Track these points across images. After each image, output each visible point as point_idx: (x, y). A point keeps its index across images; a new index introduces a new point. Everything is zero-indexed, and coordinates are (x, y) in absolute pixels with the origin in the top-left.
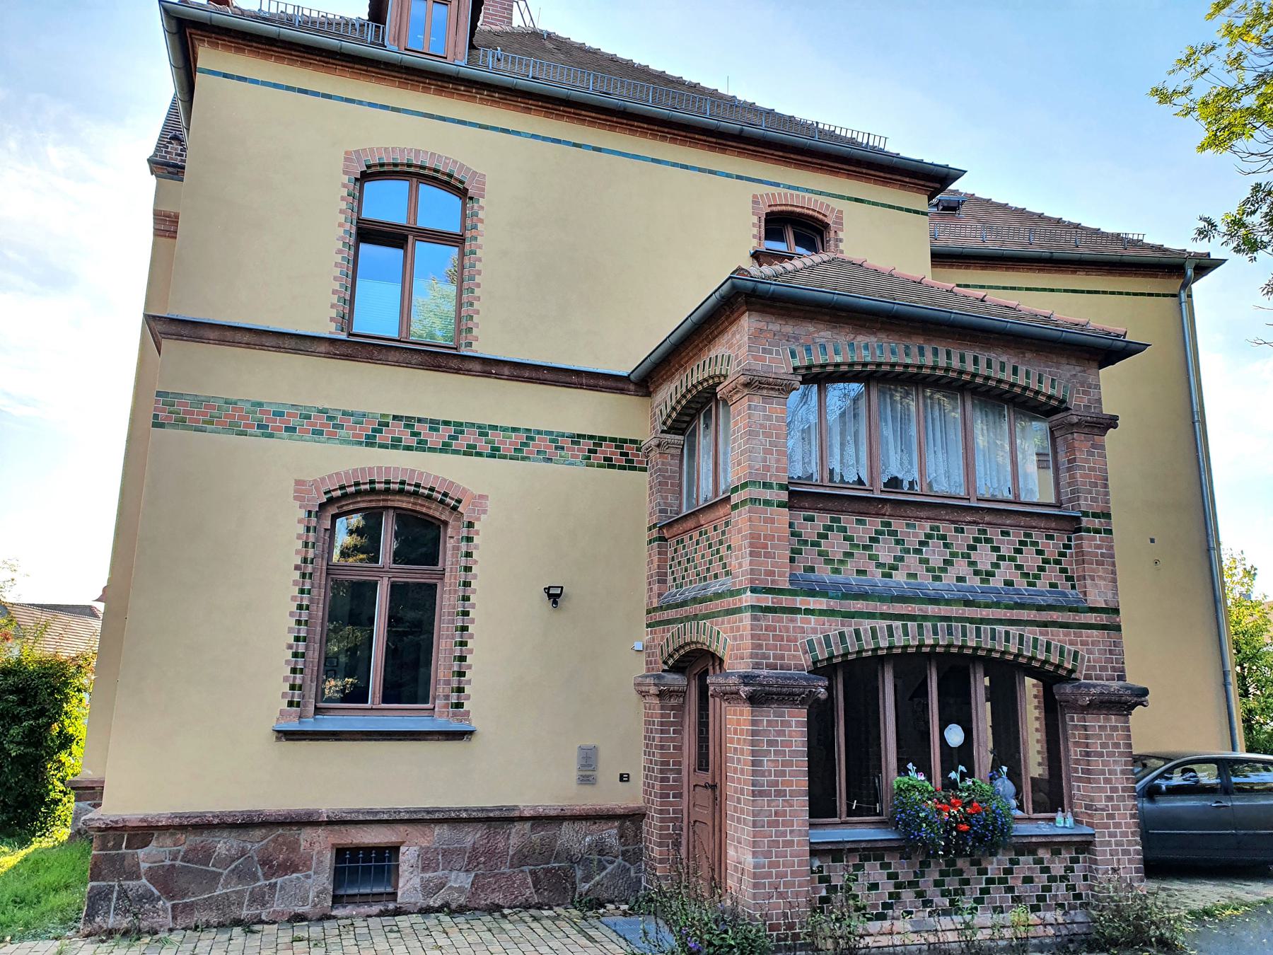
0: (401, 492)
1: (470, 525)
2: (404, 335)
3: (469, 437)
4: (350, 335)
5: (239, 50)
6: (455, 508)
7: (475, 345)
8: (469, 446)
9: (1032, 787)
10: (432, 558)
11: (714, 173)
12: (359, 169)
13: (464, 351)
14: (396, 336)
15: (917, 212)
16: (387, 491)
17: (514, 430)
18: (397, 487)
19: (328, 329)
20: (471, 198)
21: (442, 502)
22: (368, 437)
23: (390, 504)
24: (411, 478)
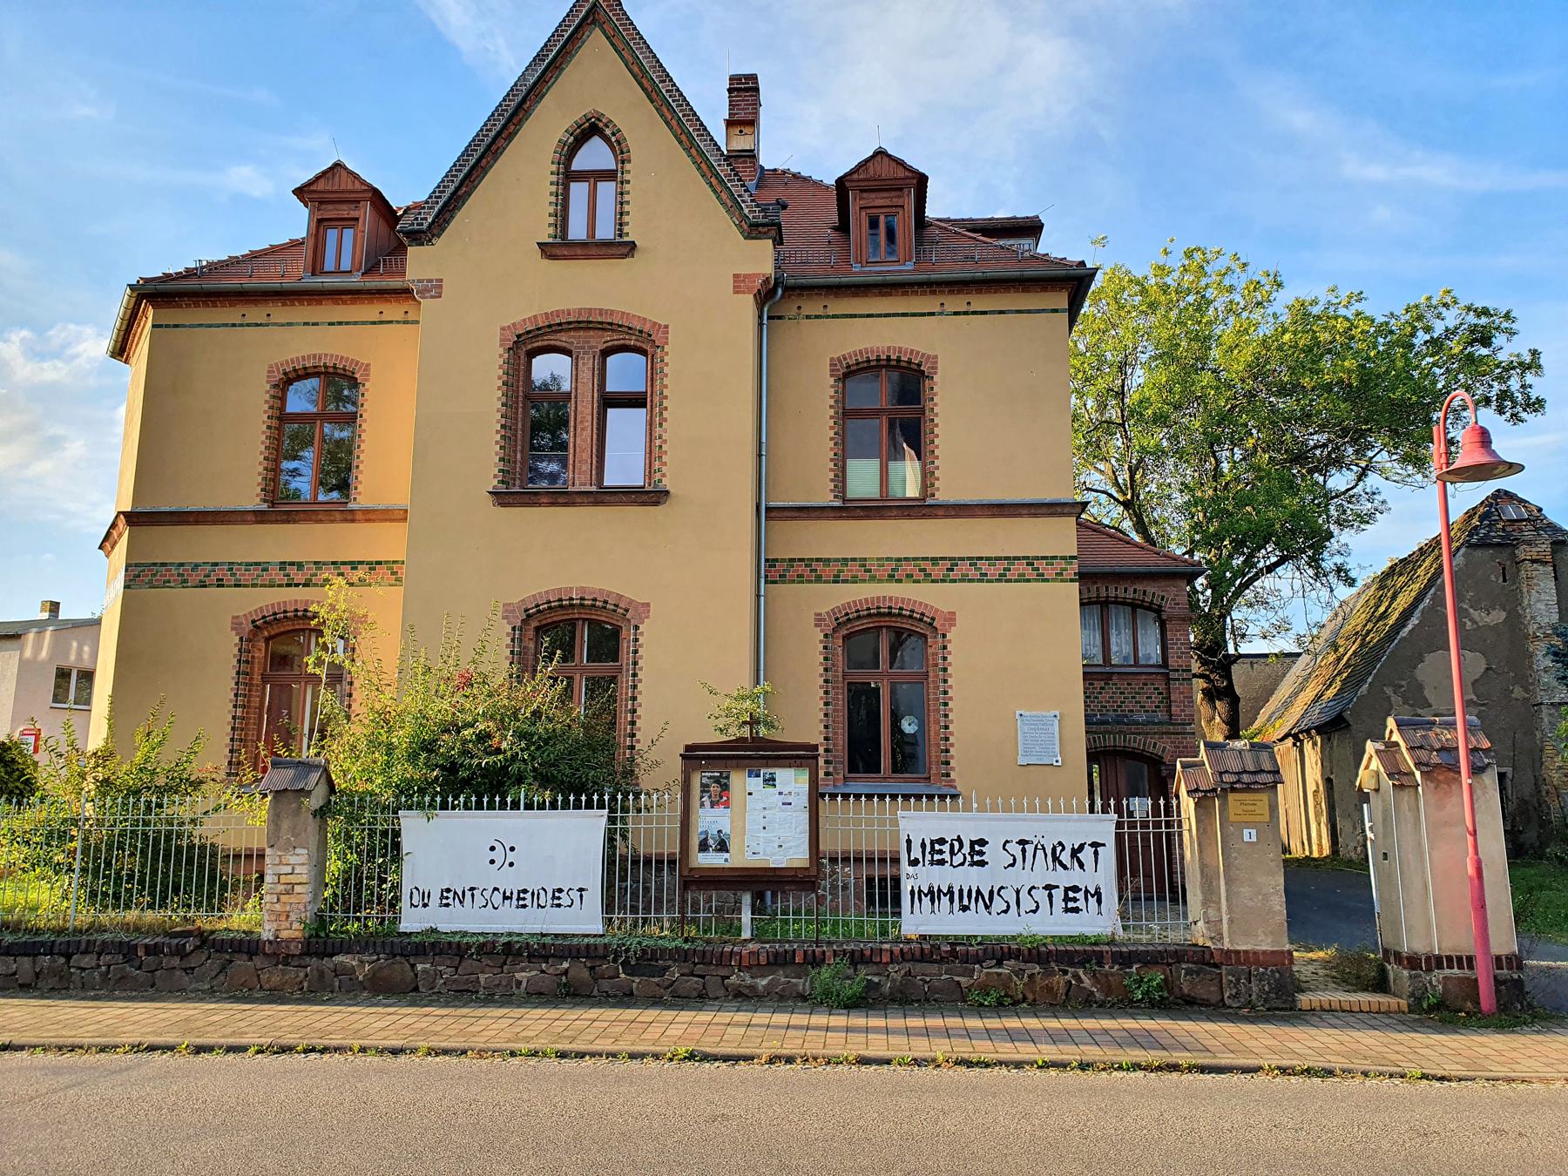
0: (859, 617)
1: (944, 636)
2: (884, 495)
3: (964, 567)
4: (844, 500)
5: (197, 305)
6: (931, 624)
7: (937, 494)
8: (356, 568)
9: (1512, 835)
10: (614, 655)
11: (855, 316)
12: (278, 376)
13: (929, 501)
14: (877, 496)
15: (257, 325)
16: (890, 614)
17: (888, 559)
18: (601, 604)
19: (827, 498)
20: (927, 377)
21: (921, 620)
22: (889, 576)
23: (882, 624)
24: (873, 604)
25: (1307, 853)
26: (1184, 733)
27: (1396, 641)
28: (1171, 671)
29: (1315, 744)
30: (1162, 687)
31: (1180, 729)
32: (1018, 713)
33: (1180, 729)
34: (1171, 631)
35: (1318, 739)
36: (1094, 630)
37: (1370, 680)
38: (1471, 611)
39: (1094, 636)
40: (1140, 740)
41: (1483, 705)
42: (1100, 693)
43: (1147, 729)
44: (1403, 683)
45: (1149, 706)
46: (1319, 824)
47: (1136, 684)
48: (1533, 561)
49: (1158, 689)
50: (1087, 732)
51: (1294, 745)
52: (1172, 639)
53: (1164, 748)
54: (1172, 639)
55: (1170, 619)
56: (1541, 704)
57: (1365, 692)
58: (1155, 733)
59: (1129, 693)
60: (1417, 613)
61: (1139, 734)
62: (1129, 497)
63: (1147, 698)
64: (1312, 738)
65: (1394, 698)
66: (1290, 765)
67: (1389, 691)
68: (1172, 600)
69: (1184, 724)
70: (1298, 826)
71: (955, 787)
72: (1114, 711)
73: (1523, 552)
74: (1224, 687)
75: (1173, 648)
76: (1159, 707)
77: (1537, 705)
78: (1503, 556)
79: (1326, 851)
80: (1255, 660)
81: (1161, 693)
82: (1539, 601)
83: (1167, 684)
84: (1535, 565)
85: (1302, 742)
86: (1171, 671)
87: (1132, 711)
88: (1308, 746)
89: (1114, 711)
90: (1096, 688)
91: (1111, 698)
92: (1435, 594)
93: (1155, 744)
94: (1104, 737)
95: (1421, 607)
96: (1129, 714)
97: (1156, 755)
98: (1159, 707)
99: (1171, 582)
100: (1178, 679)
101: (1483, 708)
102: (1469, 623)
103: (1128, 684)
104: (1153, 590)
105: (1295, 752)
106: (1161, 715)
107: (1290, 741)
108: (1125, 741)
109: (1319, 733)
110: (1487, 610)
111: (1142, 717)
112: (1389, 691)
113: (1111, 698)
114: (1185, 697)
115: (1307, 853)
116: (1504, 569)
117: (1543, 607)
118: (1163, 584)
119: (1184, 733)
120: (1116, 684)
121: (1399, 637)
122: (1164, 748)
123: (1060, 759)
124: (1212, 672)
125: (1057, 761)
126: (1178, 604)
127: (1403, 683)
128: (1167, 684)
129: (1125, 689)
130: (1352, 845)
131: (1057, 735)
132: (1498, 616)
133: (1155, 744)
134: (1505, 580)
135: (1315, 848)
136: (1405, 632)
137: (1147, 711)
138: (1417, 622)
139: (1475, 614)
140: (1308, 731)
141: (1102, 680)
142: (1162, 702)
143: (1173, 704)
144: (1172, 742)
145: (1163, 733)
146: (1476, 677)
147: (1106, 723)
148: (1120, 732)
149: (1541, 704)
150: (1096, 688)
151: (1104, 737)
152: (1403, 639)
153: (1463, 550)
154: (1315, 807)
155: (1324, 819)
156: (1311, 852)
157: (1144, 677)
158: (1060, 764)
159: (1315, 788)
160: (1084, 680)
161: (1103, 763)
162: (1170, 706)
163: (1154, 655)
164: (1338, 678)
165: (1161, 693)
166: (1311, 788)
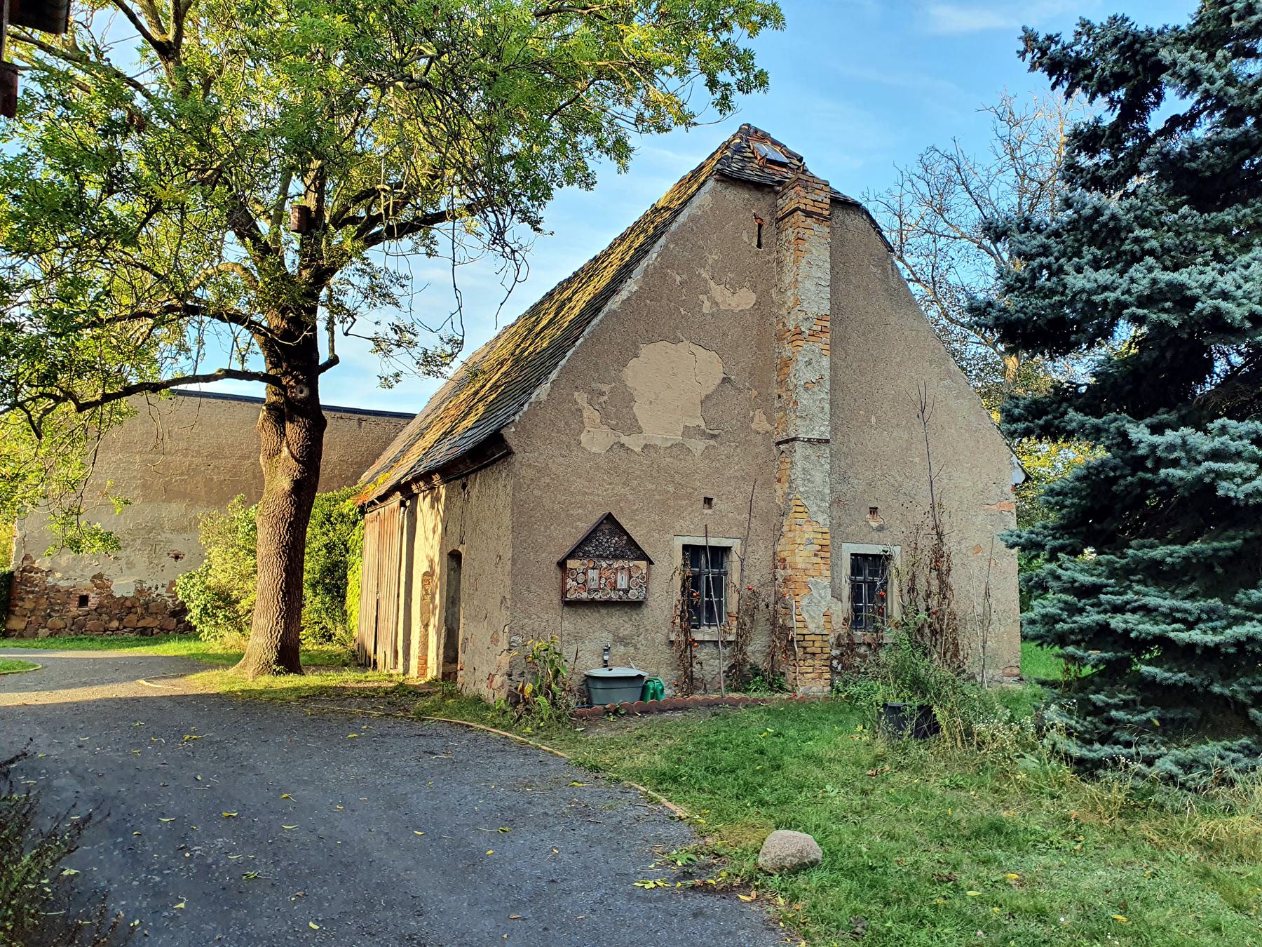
27: (601, 315)
29: (436, 500)
35: (443, 491)
37: (553, 376)
38: (712, 283)
41: (713, 436)
44: (605, 388)
46: (426, 626)
48: (809, 214)
51: (402, 504)
56: (794, 439)
57: (544, 397)
60: (638, 273)
62: (171, 37)
64: (432, 489)
65: (588, 413)
66: (392, 534)
67: (581, 398)
70: (392, 626)
73: (787, 203)
74: (300, 401)
77: (787, 442)
78: (760, 204)
79: (433, 671)
80: (365, 417)
82: (808, 277)
84: (809, 220)
85: (413, 497)
88: (423, 505)
92: (666, 246)
95: (644, 263)
101: (712, 442)
102: (707, 304)
105: (400, 517)
107: (398, 496)
109: (446, 480)
110: (732, 286)
112: (581, 398)
116: (760, 226)
117: (813, 288)
121: (606, 309)
124: (284, 374)
127: (605, 388)
130: (484, 670)
132: (745, 299)
134: (759, 246)
135: (414, 663)
136: (615, 303)
138: (636, 288)
139: (717, 290)
140: (426, 477)
146: (709, 391)
149: (794, 439)
152: (613, 313)
153: (711, 184)
154: (423, 599)
155: (434, 621)
156: (406, 671)
159: (426, 568)
164: (480, 404)
166: (420, 567)
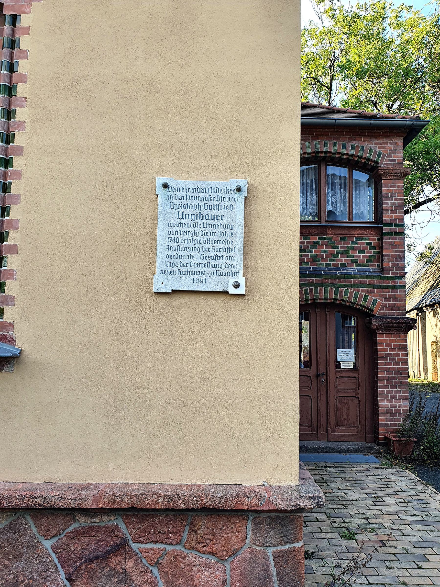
1: (14, 19)
25: (422, 377)
26: (395, 287)
28: (386, 225)
30: (375, 242)
31: (391, 282)
32: (160, 181)
33: (391, 282)
34: (386, 186)
36: (312, 190)
39: (311, 194)
40: (352, 293)
42: (314, 247)
43: (359, 281)
45: (361, 259)
47: (349, 239)
49: (371, 244)
50: (300, 285)
52: (387, 195)
53: (375, 301)
54: (387, 195)
55: (387, 174)
58: (366, 287)
59: (342, 247)
61: (350, 287)
63: (363, 252)
68: (389, 156)
69: (395, 278)
70: (416, 361)
71: (12, 341)
72: (327, 264)
75: (387, 203)
76: (371, 261)
81: (374, 248)
83: (381, 239)
86: (386, 225)
87: (345, 265)
89: (327, 264)
90: (310, 243)
91: (325, 252)
93: (366, 296)
94: (316, 290)
96: (341, 268)
97: (367, 308)
98: (371, 261)
99: (388, 140)
100: (391, 234)
103: (342, 239)
104: (372, 146)
106: (372, 270)
108: (336, 293)
111: (355, 271)
113: (325, 252)
114: (396, 251)
115: (430, 379)
118: (380, 141)
119: (395, 287)
120: (330, 239)
122: (375, 301)
123: (242, 280)
125: (237, 286)
126: (394, 161)
128: (381, 239)
129: (338, 243)
131: (239, 230)
133: (366, 296)
137: (359, 265)
141: (317, 234)
142: (374, 257)
143: (385, 259)
144: (382, 295)
145: (374, 287)
147: (319, 276)
148: (333, 285)
150: (310, 243)
151: (316, 290)
157: (357, 232)
158: (241, 291)
160: (301, 234)
161: (313, 317)
162: (382, 260)
163: (366, 213)
165: (374, 248)
